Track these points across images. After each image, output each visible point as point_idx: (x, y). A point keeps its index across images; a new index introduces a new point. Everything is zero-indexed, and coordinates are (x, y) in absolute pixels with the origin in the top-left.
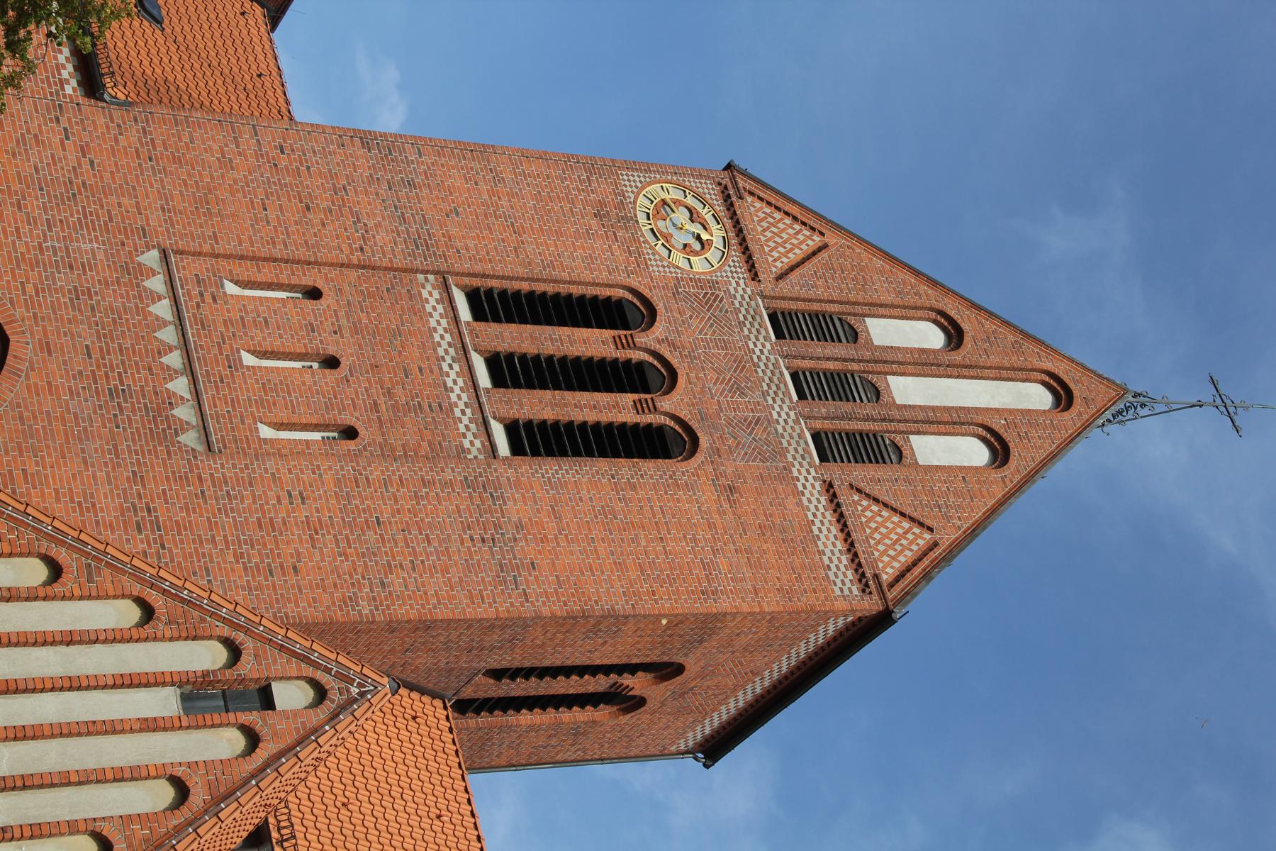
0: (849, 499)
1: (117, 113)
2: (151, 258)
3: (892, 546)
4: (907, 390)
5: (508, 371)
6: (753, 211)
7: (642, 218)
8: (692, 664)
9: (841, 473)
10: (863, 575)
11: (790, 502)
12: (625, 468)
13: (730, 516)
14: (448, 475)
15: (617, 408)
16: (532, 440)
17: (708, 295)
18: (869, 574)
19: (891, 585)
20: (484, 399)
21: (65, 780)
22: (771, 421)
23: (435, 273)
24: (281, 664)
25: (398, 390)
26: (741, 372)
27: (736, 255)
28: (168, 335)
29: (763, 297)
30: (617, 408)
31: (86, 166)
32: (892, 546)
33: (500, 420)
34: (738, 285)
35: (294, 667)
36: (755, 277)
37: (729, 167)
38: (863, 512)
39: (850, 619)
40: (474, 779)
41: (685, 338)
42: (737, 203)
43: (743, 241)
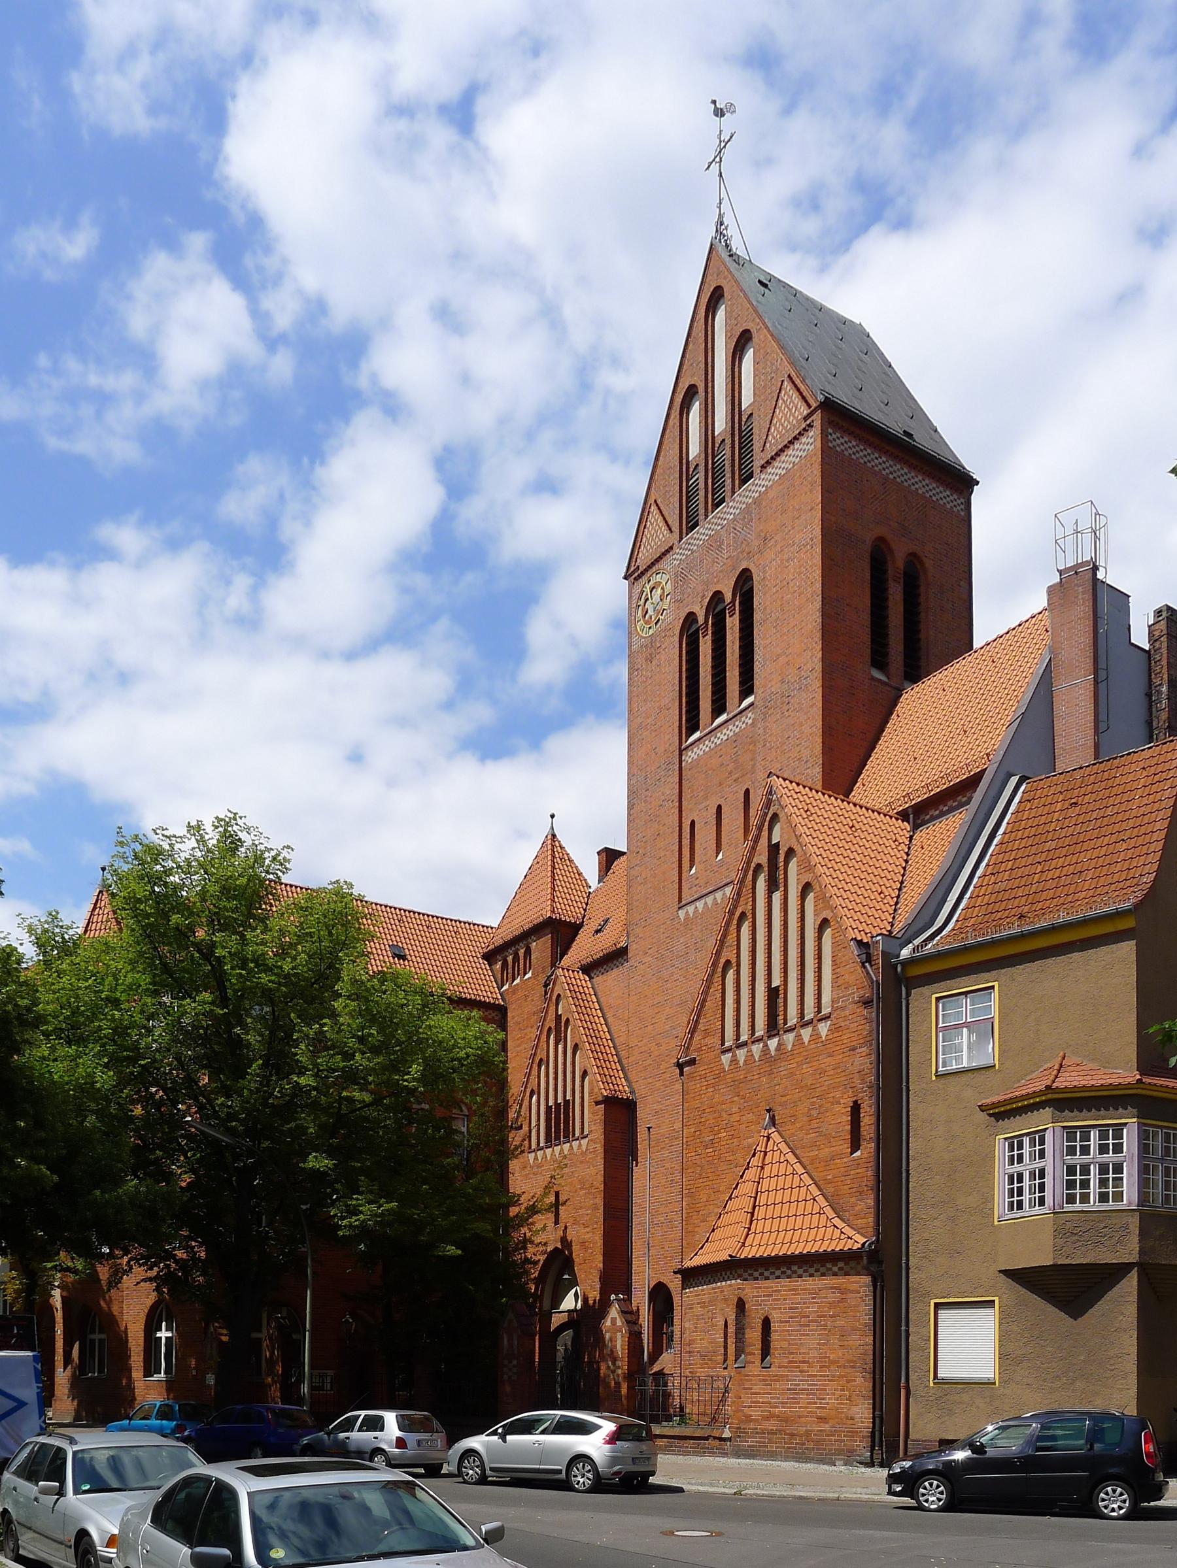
0: (770, 451)
1: (631, 939)
2: (682, 913)
3: (790, 410)
4: (721, 424)
5: (719, 707)
6: (643, 560)
7: (651, 631)
8: (869, 537)
9: (758, 460)
10: (804, 429)
11: (771, 494)
12: (757, 616)
13: (778, 538)
14: (761, 731)
15: (733, 623)
16: (747, 689)
17: (680, 578)
18: (804, 426)
19: (809, 406)
20: (731, 716)
21: (738, 1002)
22: (734, 520)
23: (680, 755)
24: (763, 843)
25: (729, 768)
26: (715, 544)
27: (662, 564)
28: (709, 900)
29: (681, 539)
30: (733, 623)
31: (650, 952)
32: (790, 410)
33: (740, 704)
34: (673, 560)
35: (765, 833)
36: (671, 548)
37: (625, 578)
38: (776, 439)
39: (830, 431)
40: (855, 796)
41: (700, 590)
42: (641, 569)
43: (657, 560)
